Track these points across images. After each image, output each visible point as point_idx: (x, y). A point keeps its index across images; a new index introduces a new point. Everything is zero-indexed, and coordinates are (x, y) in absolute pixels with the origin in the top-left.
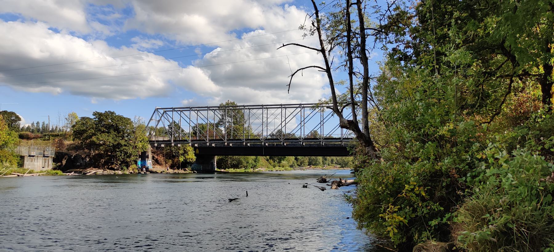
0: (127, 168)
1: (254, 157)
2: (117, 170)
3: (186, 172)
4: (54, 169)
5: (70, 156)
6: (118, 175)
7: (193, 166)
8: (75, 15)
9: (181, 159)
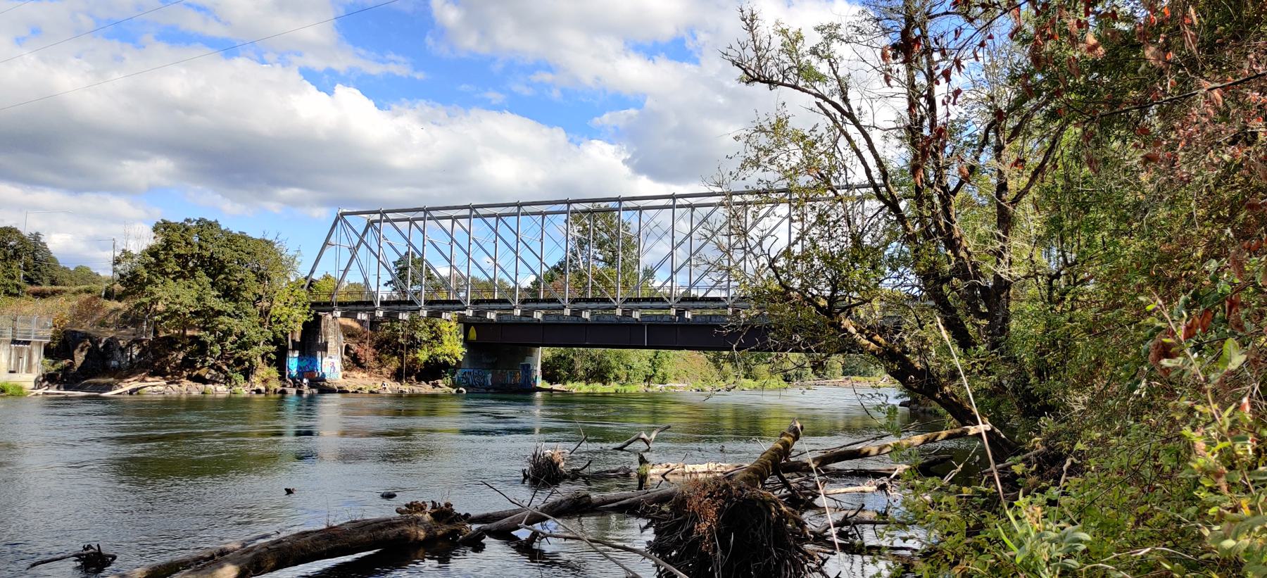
0: (247, 379)
1: (650, 353)
2: (214, 382)
3: (437, 390)
4: (50, 378)
5: (95, 341)
6: (216, 402)
7: (459, 373)
8: (313, 29)
9: (423, 355)
